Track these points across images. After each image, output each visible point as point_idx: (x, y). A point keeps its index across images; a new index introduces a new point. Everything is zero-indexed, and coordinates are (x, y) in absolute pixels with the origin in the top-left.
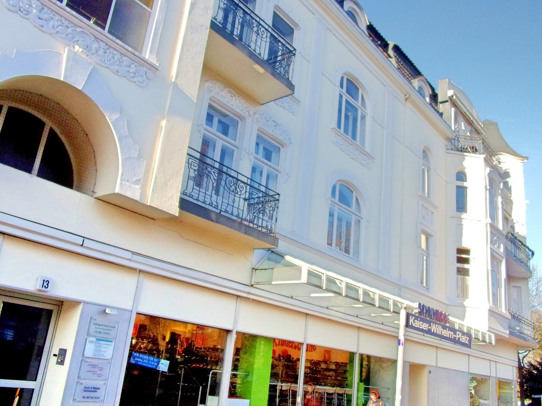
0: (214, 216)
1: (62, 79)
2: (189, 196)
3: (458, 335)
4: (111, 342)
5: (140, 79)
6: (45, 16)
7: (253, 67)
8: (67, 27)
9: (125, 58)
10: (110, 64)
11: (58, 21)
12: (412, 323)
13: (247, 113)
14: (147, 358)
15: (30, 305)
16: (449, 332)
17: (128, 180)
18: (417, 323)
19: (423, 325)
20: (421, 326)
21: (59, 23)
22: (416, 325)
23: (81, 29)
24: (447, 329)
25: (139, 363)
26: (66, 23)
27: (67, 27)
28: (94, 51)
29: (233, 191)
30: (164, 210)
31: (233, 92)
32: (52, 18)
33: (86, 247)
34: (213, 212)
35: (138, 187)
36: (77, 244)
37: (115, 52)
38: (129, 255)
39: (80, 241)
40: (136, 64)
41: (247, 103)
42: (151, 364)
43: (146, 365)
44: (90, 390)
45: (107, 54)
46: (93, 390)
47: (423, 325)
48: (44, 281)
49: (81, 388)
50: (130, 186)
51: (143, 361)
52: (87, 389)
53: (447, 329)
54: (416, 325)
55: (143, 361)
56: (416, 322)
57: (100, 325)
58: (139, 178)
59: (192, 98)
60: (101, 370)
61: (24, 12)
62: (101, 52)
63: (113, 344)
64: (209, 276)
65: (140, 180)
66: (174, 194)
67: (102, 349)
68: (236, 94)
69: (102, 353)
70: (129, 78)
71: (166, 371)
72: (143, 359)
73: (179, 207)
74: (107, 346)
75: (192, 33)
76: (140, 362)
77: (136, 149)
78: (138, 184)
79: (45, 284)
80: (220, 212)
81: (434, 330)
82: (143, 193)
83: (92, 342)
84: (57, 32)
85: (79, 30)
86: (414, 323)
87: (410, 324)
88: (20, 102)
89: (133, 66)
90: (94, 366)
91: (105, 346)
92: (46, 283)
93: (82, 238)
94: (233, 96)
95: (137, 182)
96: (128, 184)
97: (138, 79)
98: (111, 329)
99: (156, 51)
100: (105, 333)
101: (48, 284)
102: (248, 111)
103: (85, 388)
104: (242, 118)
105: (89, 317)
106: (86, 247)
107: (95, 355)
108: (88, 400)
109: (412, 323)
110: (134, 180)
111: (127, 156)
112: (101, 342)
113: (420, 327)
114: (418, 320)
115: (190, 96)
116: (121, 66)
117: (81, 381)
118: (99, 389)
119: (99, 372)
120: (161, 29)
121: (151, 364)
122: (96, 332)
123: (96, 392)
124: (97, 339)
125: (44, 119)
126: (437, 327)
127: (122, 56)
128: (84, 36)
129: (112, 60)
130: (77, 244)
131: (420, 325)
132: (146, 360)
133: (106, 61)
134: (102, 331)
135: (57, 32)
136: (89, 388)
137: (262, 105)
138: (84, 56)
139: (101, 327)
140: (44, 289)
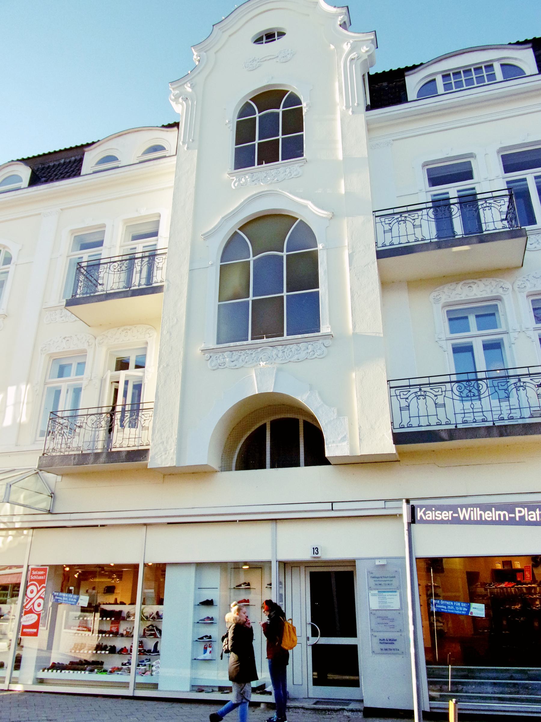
0: (444, 435)
1: (257, 393)
2: (408, 427)
3: (520, 512)
4: (396, 592)
5: (319, 352)
6: (234, 358)
7: (453, 252)
8: (252, 354)
9: (301, 345)
10: (290, 358)
11: (244, 355)
12: (421, 516)
13: (501, 289)
14: (452, 603)
15: (321, 570)
16: (497, 513)
17: (334, 442)
18: (430, 515)
19: (441, 514)
20: (439, 517)
21: (246, 355)
22: (429, 517)
23: (261, 349)
24: (493, 509)
25: (442, 610)
26: (249, 352)
27: (252, 354)
28: (275, 357)
29: (468, 396)
30: (378, 453)
31: (470, 281)
32: (240, 356)
33: (336, 510)
34: (442, 430)
35: (345, 443)
36: (328, 510)
37: (291, 346)
38: (381, 504)
39: (329, 506)
40: (311, 343)
41: (495, 279)
42: (460, 611)
43: (453, 611)
44: (386, 642)
45: (285, 353)
46: (390, 642)
47: (441, 514)
48: (313, 548)
49: (376, 641)
50: (337, 446)
51: (447, 607)
52: (383, 641)
53: (493, 509)
54: (429, 517)
55: (447, 607)
56: (429, 514)
57: (378, 578)
58: (343, 435)
59: (377, 335)
60: (392, 621)
61: (222, 365)
62: (280, 354)
63: (398, 594)
64: (476, 498)
65: (345, 437)
66: (385, 433)
67: (388, 600)
68: (475, 281)
69: (389, 604)
70: (310, 358)
71: (484, 616)
72: (447, 605)
73: (394, 444)
74: (392, 597)
75: (358, 279)
76: (444, 609)
77: (333, 412)
78: (345, 441)
79: (315, 551)
80: (456, 427)
81: (464, 517)
82: (352, 448)
83: (374, 595)
84: (246, 362)
85: (259, 350)
86: (425, 516)
87: (419, 518)
88: (275, 413)
89: (310, 346)
90: (383, 618)
91: (390, 597)
92: (316, 550)
93: (331, 503)
94: (472, 285)
95: (344, 439)
96: (334, 445)
97: (318, 353)
98: (391, 579)
99: (328, 320)
100: (385, 584)
101: (317, 551)
102: (501, 287)
103: (380, 640)
104: (498, 299)
105: (70, 581)
106: (336, 510)
107: (380, 606)
108: (386, 652)
109: (421, 516)
110: (340, 439)
111: (327, 421)
112: (384, 594)
113: (437, 518)
114: (432, 511)
115: (374, 335)
116: (300, 353)
117: (376, 634)
118: (395, 640)
119: (391, 624)
120: (327, 299)
121: (460, 611)
122: (376, 585)
123: (394, 643)
124: (379, 592)
125: (296, 416)
126: (471, 510)
127: (298, 345)
128: (265, 351)
129: (291, 354)
130: (328, 510)
131: (436, 516)
132: (451, 605)
133: (286, 357)
134: (382, 583)
135: (246, 362)
136: (384, 640)
137: (522, 266)
138: (270, 366)
139: (380, 579)
140: (315, 555)
